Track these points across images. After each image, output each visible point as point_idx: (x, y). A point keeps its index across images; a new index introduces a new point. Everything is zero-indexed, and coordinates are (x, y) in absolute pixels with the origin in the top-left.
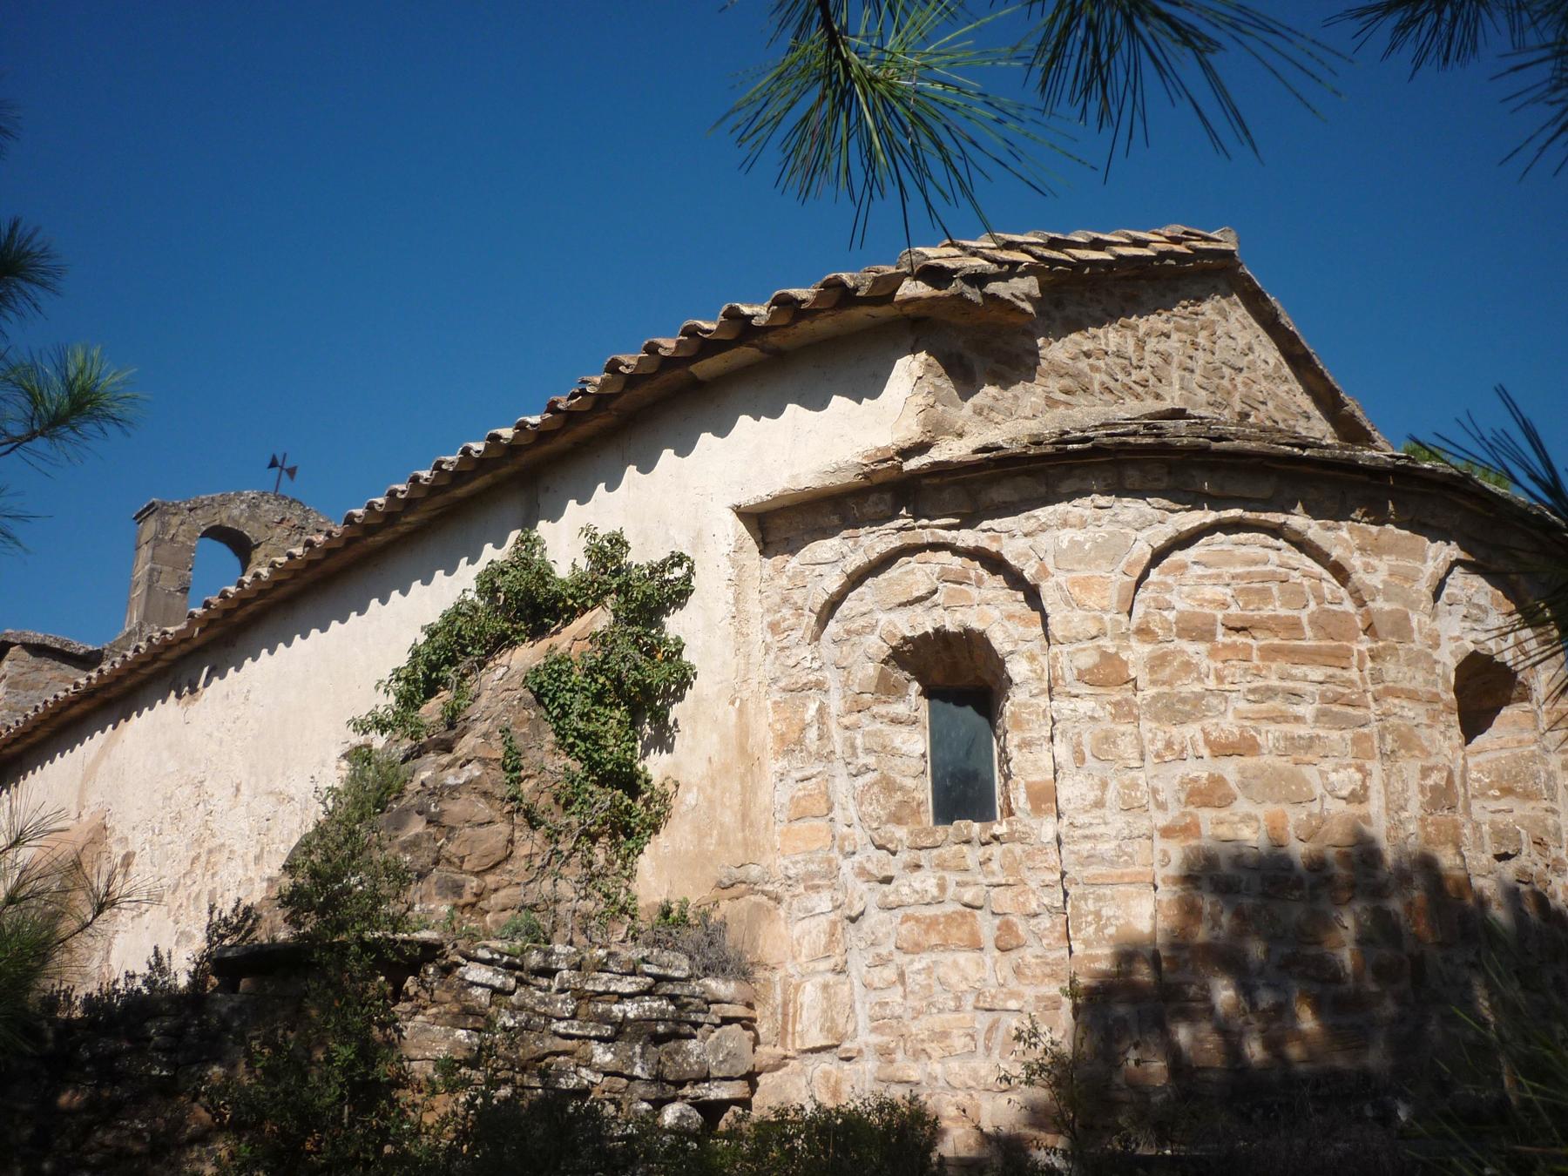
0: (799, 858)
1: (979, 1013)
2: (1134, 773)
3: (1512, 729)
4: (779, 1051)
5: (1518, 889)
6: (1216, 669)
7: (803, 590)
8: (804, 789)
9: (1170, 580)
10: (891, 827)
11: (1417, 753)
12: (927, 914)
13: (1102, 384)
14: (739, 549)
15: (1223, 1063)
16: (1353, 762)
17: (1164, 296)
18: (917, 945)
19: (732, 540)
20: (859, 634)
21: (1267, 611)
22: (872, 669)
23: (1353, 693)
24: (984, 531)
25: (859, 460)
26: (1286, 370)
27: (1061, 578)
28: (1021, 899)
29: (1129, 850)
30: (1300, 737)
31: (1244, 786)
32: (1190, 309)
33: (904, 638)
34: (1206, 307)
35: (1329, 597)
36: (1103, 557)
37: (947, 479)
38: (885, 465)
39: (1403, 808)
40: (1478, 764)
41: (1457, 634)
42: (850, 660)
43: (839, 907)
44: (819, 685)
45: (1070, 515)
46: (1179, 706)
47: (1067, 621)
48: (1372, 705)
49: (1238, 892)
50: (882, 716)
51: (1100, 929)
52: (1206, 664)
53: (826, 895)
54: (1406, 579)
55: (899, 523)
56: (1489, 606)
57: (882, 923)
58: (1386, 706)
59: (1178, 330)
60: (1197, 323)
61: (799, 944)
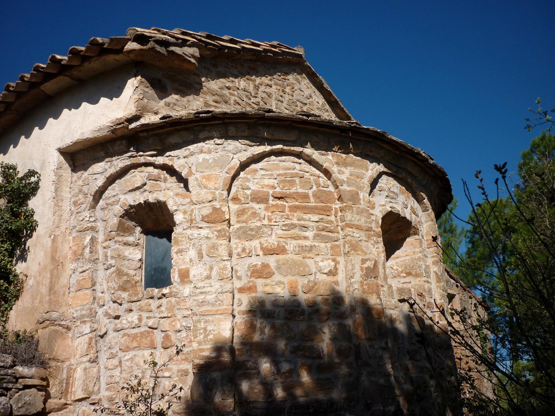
0: (78, 308)
2: (226, 263)
3: (411, 247)
4: (63, 401)
5: (409, 315)
6: (268, 216)
7: (88, 186)
8: (82, 276)
9: (249, 177)
10: (119, 292)
11: (360, 252)
13: (235, 101)
14: (60, 168)
15: (263, 399)
16: (331, 257)
17: (269, 70)
18: (128, 347)
19: (56, 164)
20: (112, 205)
21: (293, 190)
22: (116, 220)
23: (332, 227)
24: (167, 157)
25: (109, 124)
26: (327, 107)
27: (198, 175)
28: (173, 324)
29: (221, 298)
30: (306, 246)
31: (278, 268)
32: (282, 77)
33: (130, 205)
34: (290, 77)
35: (322, 185)
36: (218, 166)
37: (151, 133)
38: (120, 126)
39: (352, 277)
40: (397, 263)
41: (383, 203)
42: (107, 217)
43: (95, 330)
44: (93, 229)
45: (204, 148)
46: (249, 232)
47: (198, 194)
48: (341, 232)
49: (274, 317)
50: (120, 242)
51: (206, 336)
52: (263, 213)
53: (88, 325)
54: (358, 177)
55: (129, 154)
56: (398, 192)
57: (114, 338)
58: (346, 232)
59: (276, 84)
60: (285, 83)
61: (77, 349)
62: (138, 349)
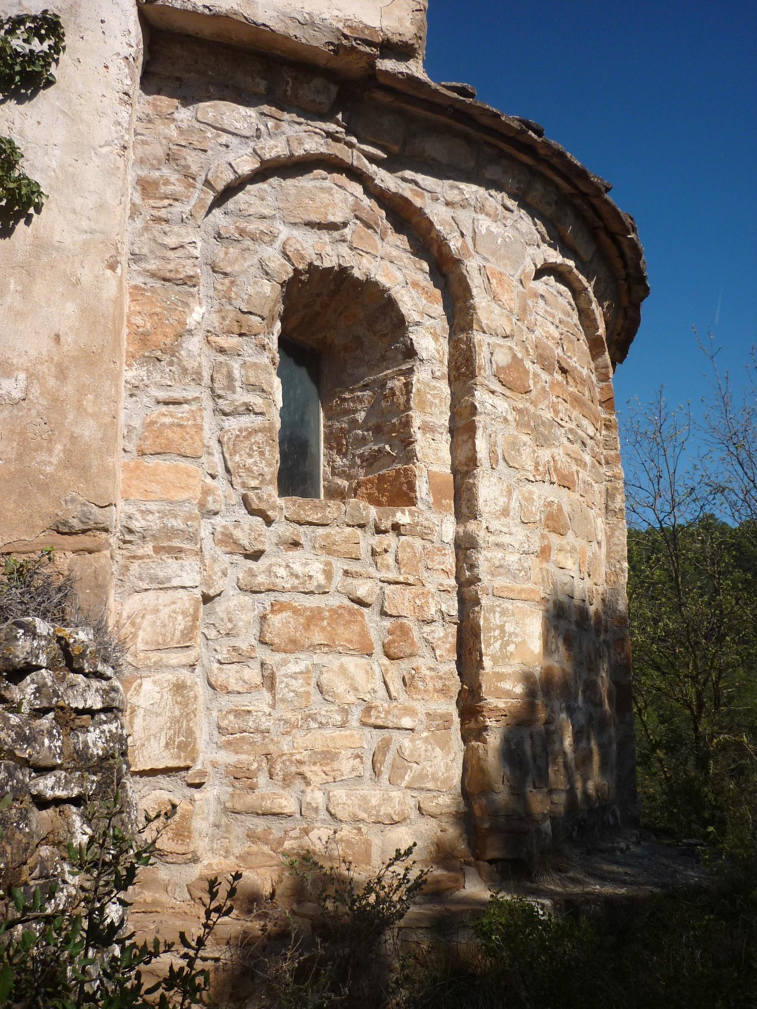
0: (153, 507)
1: (367, 730)
12: (307, 605)
18: (294, 642)
24: (404, 180)
25: (340, 26)
38: (367, 49)
42: (237, 268)
55: (332, 127)
57: (242, 608)
62: (326, 649)
